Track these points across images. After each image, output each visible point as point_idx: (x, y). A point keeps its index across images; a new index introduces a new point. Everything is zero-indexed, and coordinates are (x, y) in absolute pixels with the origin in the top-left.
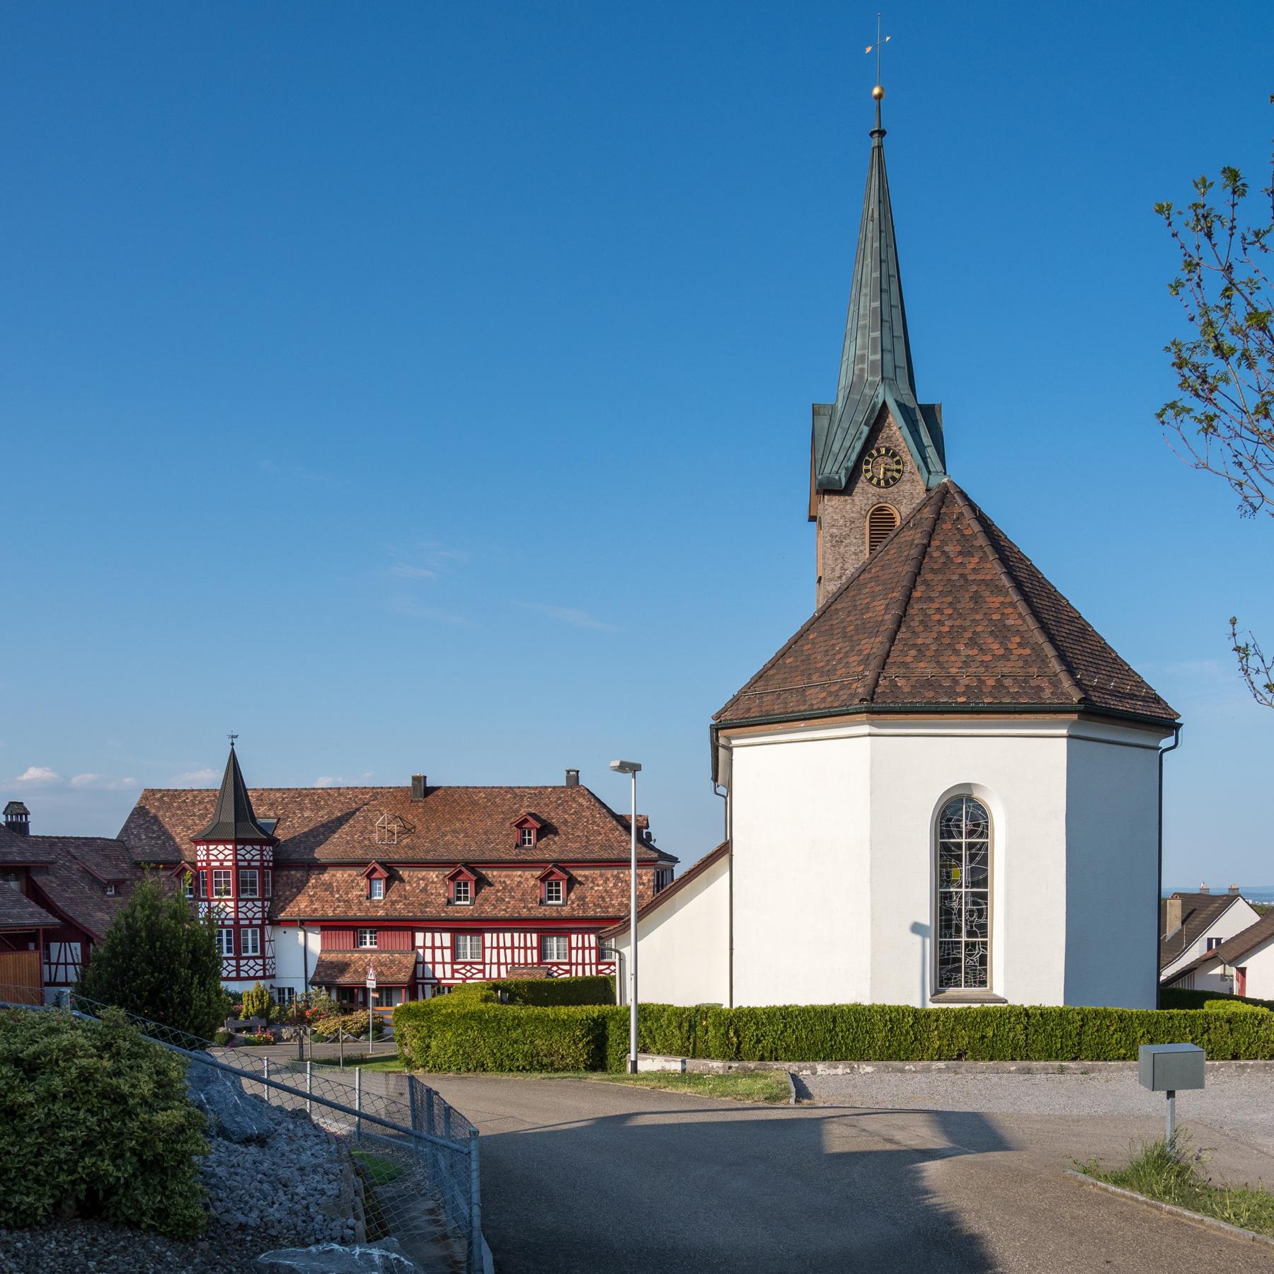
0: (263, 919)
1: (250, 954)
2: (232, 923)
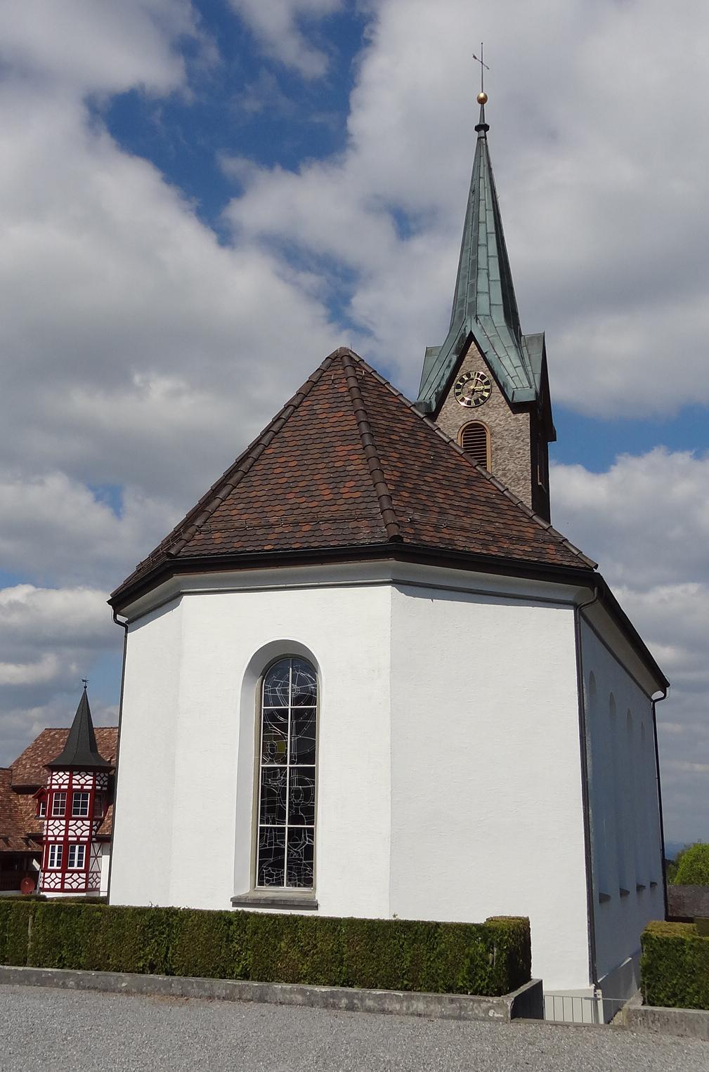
0: (90, 837)
1: (75, 867)
2: (62, 839)
